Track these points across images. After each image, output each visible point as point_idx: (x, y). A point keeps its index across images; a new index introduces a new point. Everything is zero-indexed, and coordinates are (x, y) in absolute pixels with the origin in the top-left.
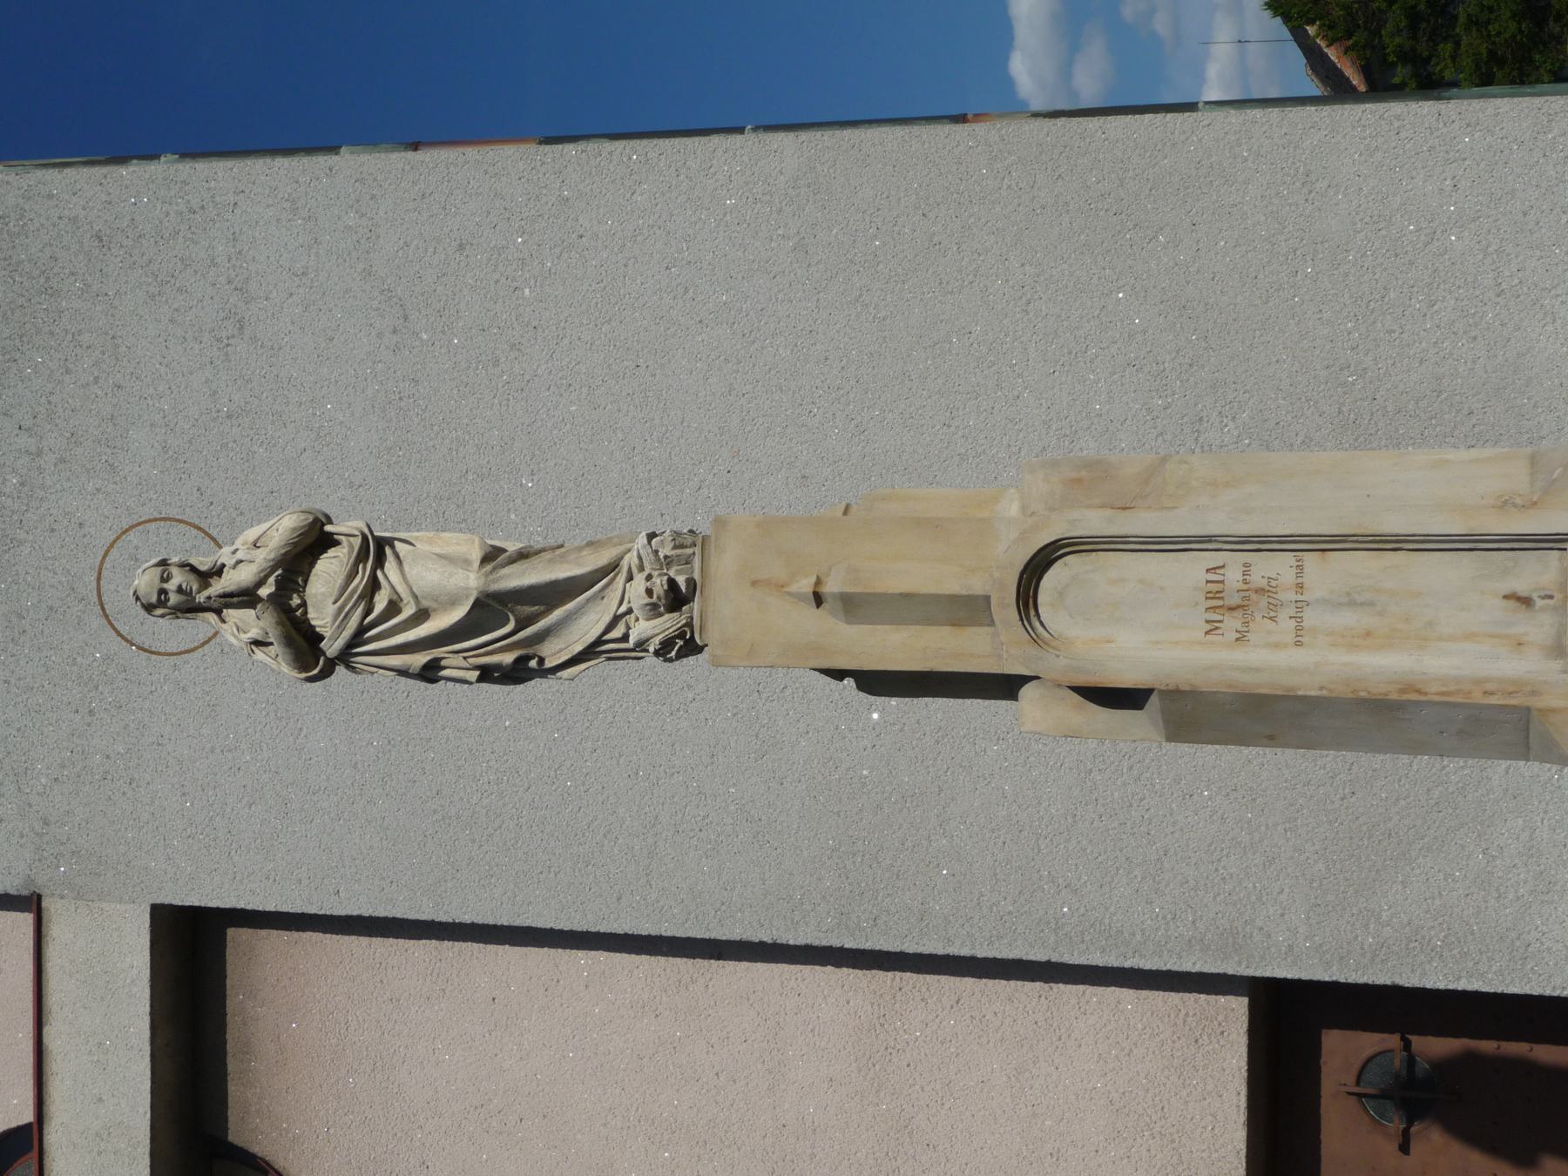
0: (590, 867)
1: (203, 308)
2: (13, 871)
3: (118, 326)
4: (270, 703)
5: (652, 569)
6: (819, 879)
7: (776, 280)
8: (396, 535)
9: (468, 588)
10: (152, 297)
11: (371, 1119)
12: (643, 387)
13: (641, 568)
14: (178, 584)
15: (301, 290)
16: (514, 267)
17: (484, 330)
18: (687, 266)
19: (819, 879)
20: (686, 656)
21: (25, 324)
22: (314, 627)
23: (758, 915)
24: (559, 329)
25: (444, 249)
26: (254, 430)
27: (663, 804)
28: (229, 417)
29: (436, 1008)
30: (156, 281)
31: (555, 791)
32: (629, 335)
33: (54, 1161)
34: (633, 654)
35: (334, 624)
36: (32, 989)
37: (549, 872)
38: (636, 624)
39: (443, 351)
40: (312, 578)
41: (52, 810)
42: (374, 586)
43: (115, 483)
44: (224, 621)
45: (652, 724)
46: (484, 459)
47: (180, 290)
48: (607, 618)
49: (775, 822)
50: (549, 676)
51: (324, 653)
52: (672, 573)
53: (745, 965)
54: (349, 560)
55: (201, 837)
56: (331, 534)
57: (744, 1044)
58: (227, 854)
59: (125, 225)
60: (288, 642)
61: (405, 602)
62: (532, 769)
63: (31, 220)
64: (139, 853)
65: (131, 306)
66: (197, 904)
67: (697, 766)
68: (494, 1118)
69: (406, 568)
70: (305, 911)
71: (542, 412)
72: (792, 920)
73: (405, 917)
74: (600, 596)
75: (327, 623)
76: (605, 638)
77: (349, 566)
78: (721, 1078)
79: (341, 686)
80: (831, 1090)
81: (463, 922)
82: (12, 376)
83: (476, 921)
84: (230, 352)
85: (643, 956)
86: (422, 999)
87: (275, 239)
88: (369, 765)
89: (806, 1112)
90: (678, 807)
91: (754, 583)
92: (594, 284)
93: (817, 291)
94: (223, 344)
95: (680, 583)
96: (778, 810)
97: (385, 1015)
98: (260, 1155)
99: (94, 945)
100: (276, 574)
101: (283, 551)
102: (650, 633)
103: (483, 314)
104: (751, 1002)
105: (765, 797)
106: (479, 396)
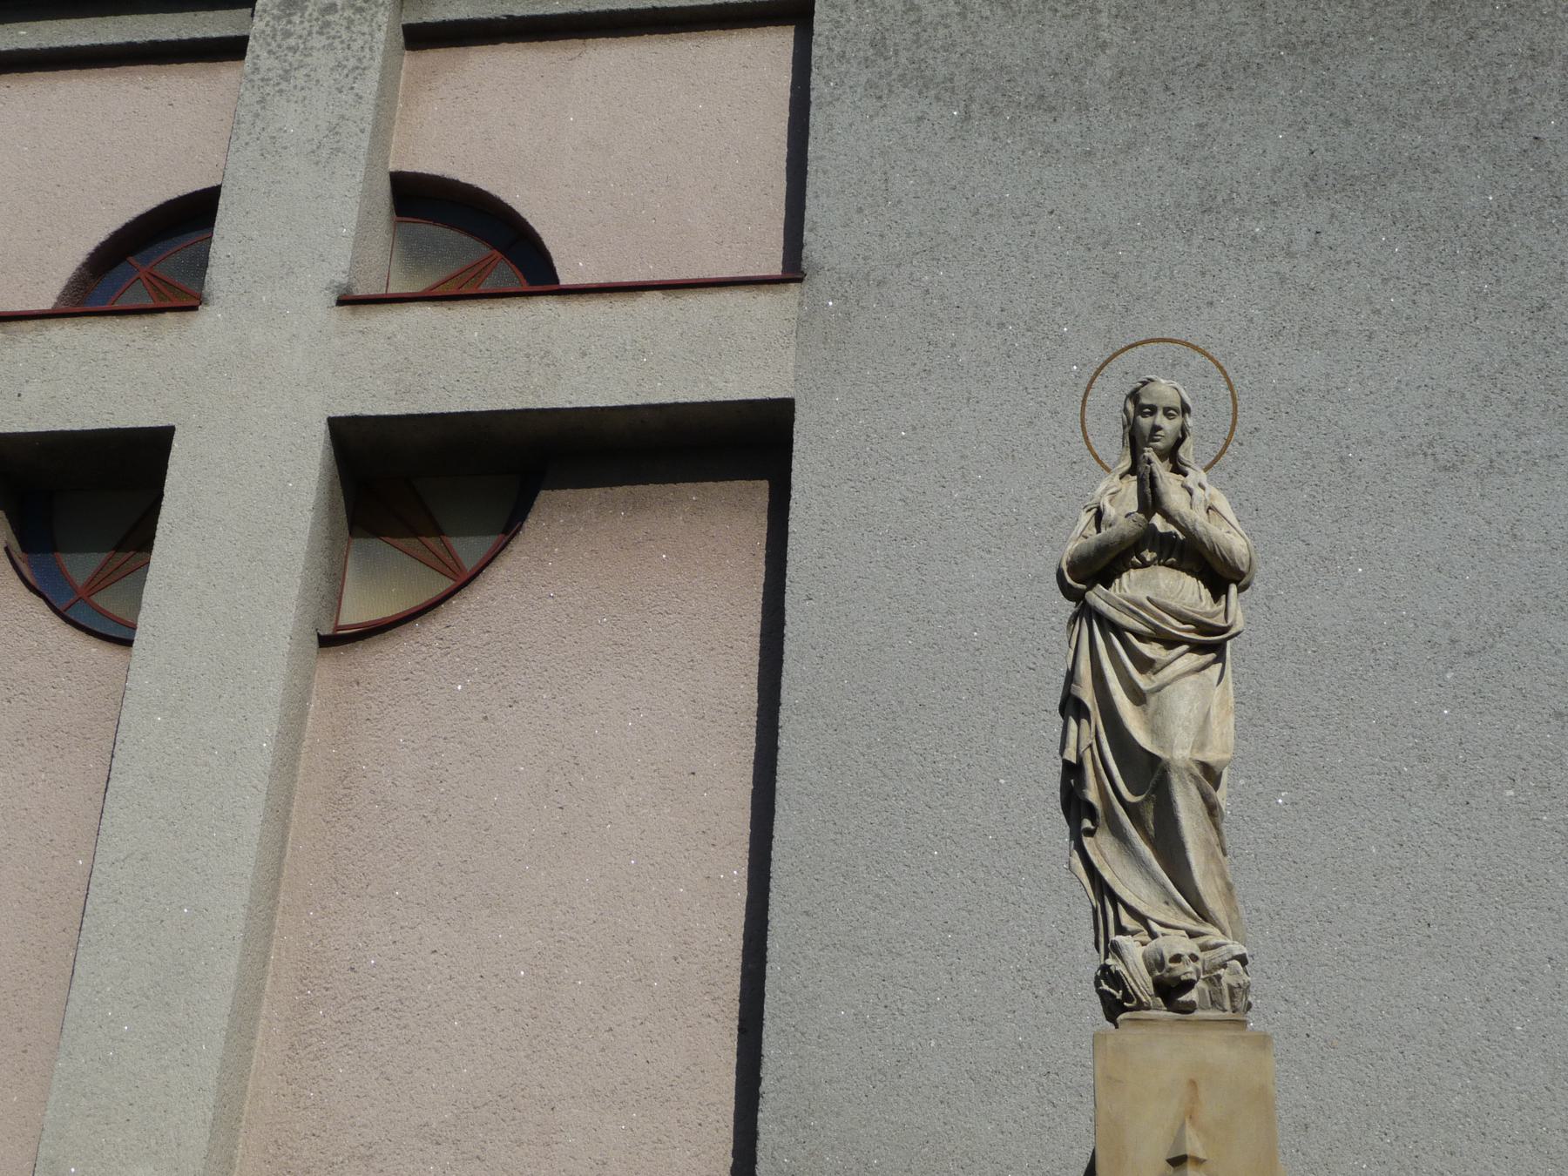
0: (842, 879)
1: (1467, 425)
2: (827, 251)
3: (1441, 332)
4: (1018, 517)
5: (1204, 961)
6: (833, 1148)
7: (1544, 1090)
8: (1228, 664)
9: (1172, 748)
10: (1477, 369)
11: (562, 642)
12: (1404, 931)
13: (1204, 948)
14: (1162, 426)
15: (1494, 534)
16: (1539, 776)
17: (1461, 743)
18: (1554, 983)
19: (833, 1148)
20: (1103, 1002)
21: (1437, 231)
22: (1120, 576)
23: (791, 1076)
24: (1468, 831)
25: (1555, 696)
26: (1328, 488)
27: (915, 962)
28: (1342, 460)
29: (684, 710)
30: (1495, 372)
31: (927, 837)
32: (1466, 915)
33: (519, 308)
34: (1102, 939)
35: (1124, 599)
36: (701, 277)
37: (836, 833)
38: (1139, 943)
39: (1433, 697)
40: (1175, 573)
41: (894, 289)
42: (1170, 642)
43: (1259, 339)
44: (1122, 477)
45: (1007, 947)
46: (1308, 747)
47: (1487, 399)
48: (1142, 908)
49: (898, 1095)
50: (1073, 842)
51: (1090, 588)
52: (1200, 984)
53: (734, 1060)
54: (1198, 613)
55: (868, 449)
56: (1227, 592)
57: (645, 1061)
58: (850, 477)
59: (1559, 335)
60: (1102, 549)
61: (1153, 677)
62: (951, 810)
63: (1558, 232)
64: (849, 383)
65: (1464, 346)
66: (795, 447)
67: (960, 1001)
68: (564, 777)
69: (1193, 678)
70: (788, 564)
71: (1368, 813)
72: (785, 1117)
73: (784, 673)
74: (1169, 900)
75: (1125, 592)
76: (1120, 907)
77: (1191, 614)
78: (606, 1034)
79: (1038, 594)
80: (593, 1163)
81: (779, 738)
82: (1376, 220)
83: (780, 751)
84: (1417, 457)
85: (742, 942)
86: (692, 694)
87: (1554, 502)
88: (950, 628)
89: (568, 1134)
90: (912, 979)
91: (1193, 1084)
92: (1525, 871)
93: (1534, 1141)
94: (1426, 449)
95: (1188, 994)
96: (911, 1098)
97: (676, 654)
98: (525, 525)
99: (749, 340)
100: (1178, 533)
101: (1205, 540)
102: (1129, 959)
103: (1480, 741)
104: (692, 1068)
105: (926, 1082)
106: (1382, 739)
